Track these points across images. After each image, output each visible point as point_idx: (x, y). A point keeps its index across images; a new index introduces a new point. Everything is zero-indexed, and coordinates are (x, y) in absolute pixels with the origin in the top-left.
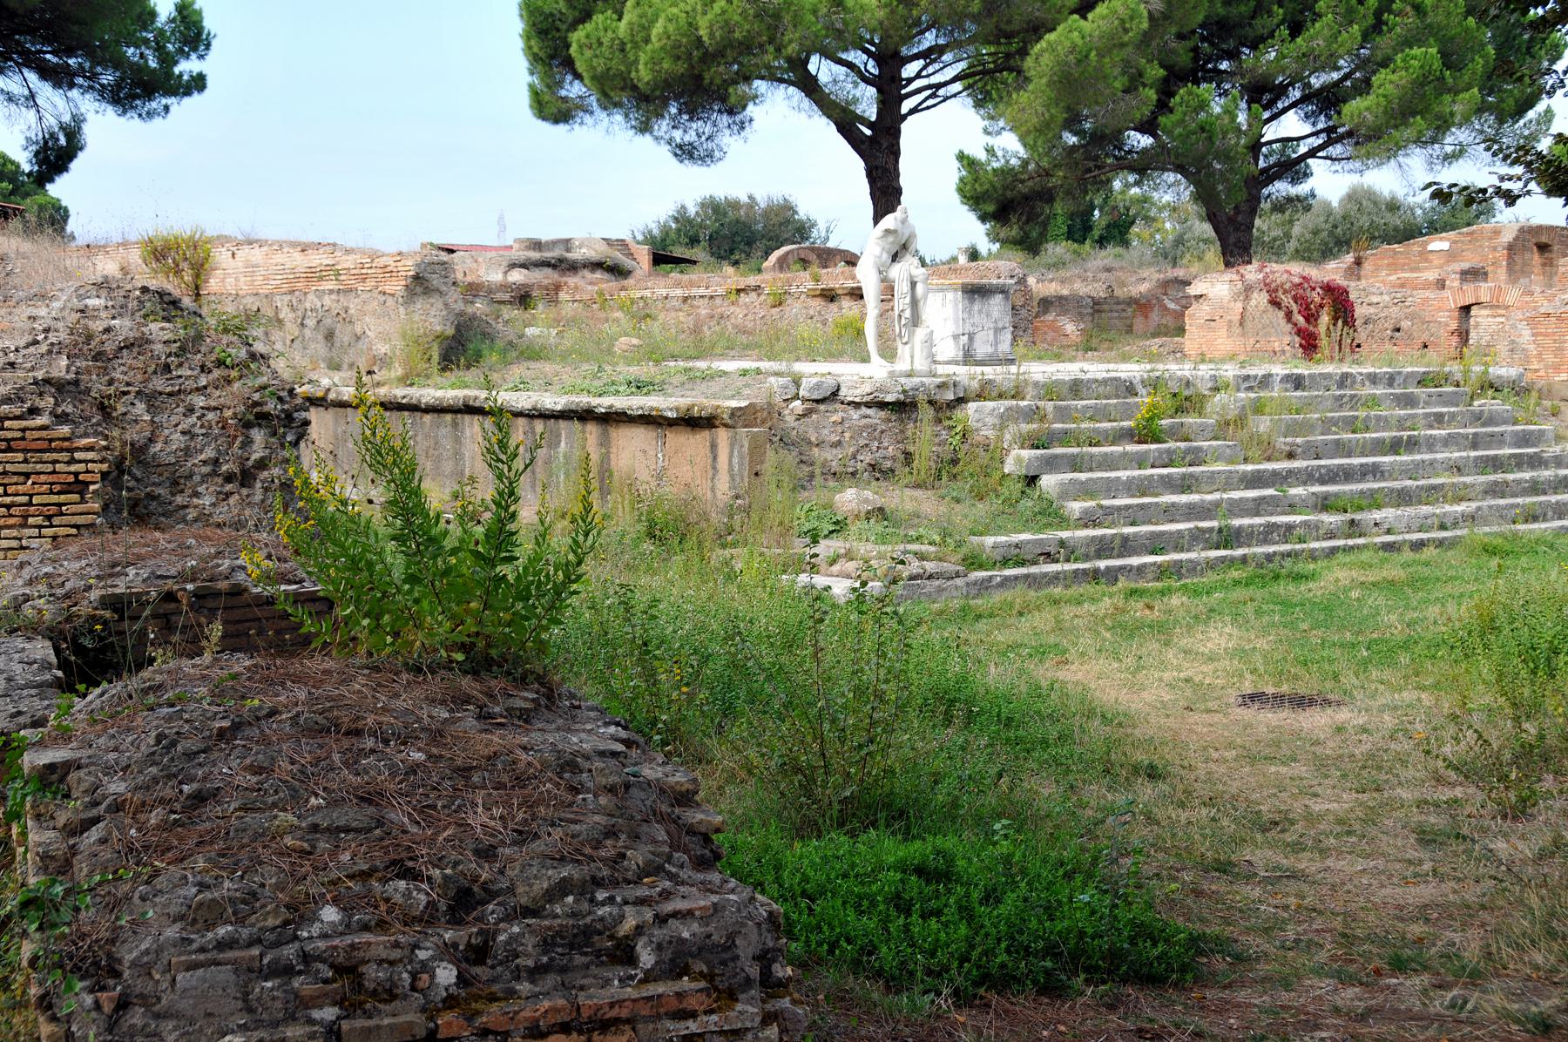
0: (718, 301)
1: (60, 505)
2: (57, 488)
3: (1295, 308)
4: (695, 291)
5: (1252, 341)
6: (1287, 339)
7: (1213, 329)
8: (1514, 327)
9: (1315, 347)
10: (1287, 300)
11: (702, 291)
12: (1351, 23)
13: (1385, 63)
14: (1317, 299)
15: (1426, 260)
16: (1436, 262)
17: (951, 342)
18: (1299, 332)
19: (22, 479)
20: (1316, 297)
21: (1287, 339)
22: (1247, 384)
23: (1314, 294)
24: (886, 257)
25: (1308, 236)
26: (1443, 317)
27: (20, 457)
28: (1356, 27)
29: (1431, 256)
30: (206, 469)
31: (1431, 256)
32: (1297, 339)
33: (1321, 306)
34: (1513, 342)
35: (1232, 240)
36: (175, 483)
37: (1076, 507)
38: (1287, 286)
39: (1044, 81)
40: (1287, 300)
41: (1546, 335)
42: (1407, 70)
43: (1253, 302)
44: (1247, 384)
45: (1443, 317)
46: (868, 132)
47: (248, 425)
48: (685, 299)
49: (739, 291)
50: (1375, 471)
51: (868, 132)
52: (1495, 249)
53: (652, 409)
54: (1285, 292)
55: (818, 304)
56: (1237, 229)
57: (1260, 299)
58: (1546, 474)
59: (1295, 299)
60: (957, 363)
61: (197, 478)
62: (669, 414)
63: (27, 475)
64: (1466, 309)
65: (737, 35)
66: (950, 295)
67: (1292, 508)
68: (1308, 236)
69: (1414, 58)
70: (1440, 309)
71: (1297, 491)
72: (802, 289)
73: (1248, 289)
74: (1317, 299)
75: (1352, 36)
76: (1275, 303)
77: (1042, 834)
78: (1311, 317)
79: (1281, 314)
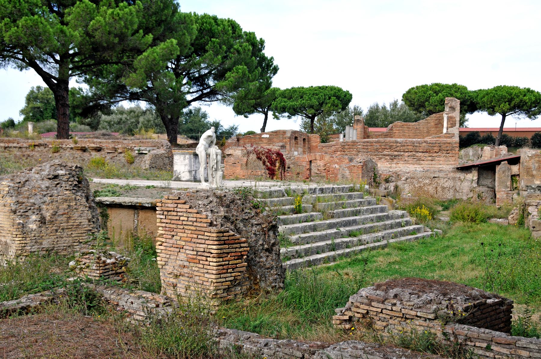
0: (24, 149)
1: (236, 264)
2: (236, 258)
3: (266, 160)
4: (10, 145)
5: (250, 171)
6: (263, 171)
7: (235, 167)
8: (343, 170)
9: (274, 174)
10: (264, 157)
11: (15, 145)
12: (217, 55)
13: (230, 69)
14: (275, 158)
15: (261, 141)
16: (265, 142)
17: (188, 174)
18: (268, 169)
19: (226, 255)
20: (274, 156)
21: (263, 171)
22: (310, 192)
23: (273, 156)
24: (207, 145)
25: (146, 122)
26: (304, 164)
27: (227, 246)
28: (220, 56)
29: (263, 139)
30: (261, 248)
31: (263, 139)
32: (267, 172)
33: (277, 160)
34: (343, 175)
35: (170, 128)
36: (255, 254)
37: (294, 238)
38: (263, 153)
39: (143, 70)
40: (264, 157)
41: (354, 173)
42: (237, 73)
43: (250, 158)
44: (310, 192)
45: (304, 164)
46: (55, 82)
47: (269, 230)
48: (5, 148)
49: (35, 146)
50: (355, 222)
51: (55, 82)
52: (285, 138)
53: (137, 203)
54: (263, 154)
55: (79, 153)
56: (172, 124)
57: (253, 157)
58: (388, 222)
59: (267, 157)
60: (191, 181)
61: (260, 251)
62: (147, 205)
63: (228, 253)
64: (311, 161)
65: (22, 42)
66: (187, 156)
67: (343, 236)
68: (146, 122)
69: (240, 69)
70: (303, 161)
71: (342, 229)
72: (68, 146)
73: (248, 153)
74: (275, 158)
75: (218, 60)
76: (259, 158)
77: (124, 347)
78: (273, 163)
79: (261, 162)
